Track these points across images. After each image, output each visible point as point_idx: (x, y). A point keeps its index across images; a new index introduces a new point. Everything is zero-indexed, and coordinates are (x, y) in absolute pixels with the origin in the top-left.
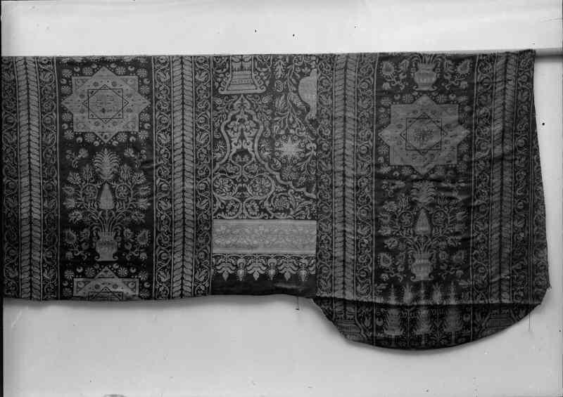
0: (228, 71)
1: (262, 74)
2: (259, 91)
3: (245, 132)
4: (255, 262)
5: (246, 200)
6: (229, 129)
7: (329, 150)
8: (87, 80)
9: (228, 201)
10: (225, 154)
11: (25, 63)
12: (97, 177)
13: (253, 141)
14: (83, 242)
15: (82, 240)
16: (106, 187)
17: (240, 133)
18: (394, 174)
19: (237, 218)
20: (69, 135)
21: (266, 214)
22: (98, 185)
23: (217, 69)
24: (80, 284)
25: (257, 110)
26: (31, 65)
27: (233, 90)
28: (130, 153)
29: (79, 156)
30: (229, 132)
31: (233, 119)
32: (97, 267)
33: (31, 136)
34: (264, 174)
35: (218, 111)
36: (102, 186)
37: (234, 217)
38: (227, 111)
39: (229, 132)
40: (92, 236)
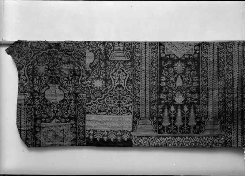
0: (113, 50)
1: (128, 52)
2: (127, 60)
3: (121, 77)
4: (125, 134)
5: (121, 107)
6: (113, 76)
7: (207, 76)
9: (113, 107)
10: (112, 86)
12: (175, 73)
13: (125, 81)
16: (179, 76)
17: (118, 78)
18: (69, 120)
19: (117, 115)
20: (163, 55)
21: (130, 113)
22: (176, 76)
23: (108, 49)
25: (126, 68)
27: (116, 59)
28: (190, 63)
29: (168, 64)
30: (113, 77)
31: (116, 71)
34: (129, 96)
35: (109, 67)
36: (177, 76)
37: (116, 114)
38: (113, 68)
39: (113, 77)
40: (172, 96)
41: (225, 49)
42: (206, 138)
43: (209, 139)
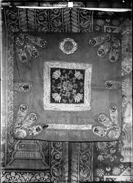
8: (115, 29)
11: (71, 13)
14: (111, 148)
15: (110, 146)
24: (109, 30)
26: (74, 5)
32: (122, 167)
33: (72, 18)
41: (48, 21)
42: (16, 174)
43: (22, 177)
